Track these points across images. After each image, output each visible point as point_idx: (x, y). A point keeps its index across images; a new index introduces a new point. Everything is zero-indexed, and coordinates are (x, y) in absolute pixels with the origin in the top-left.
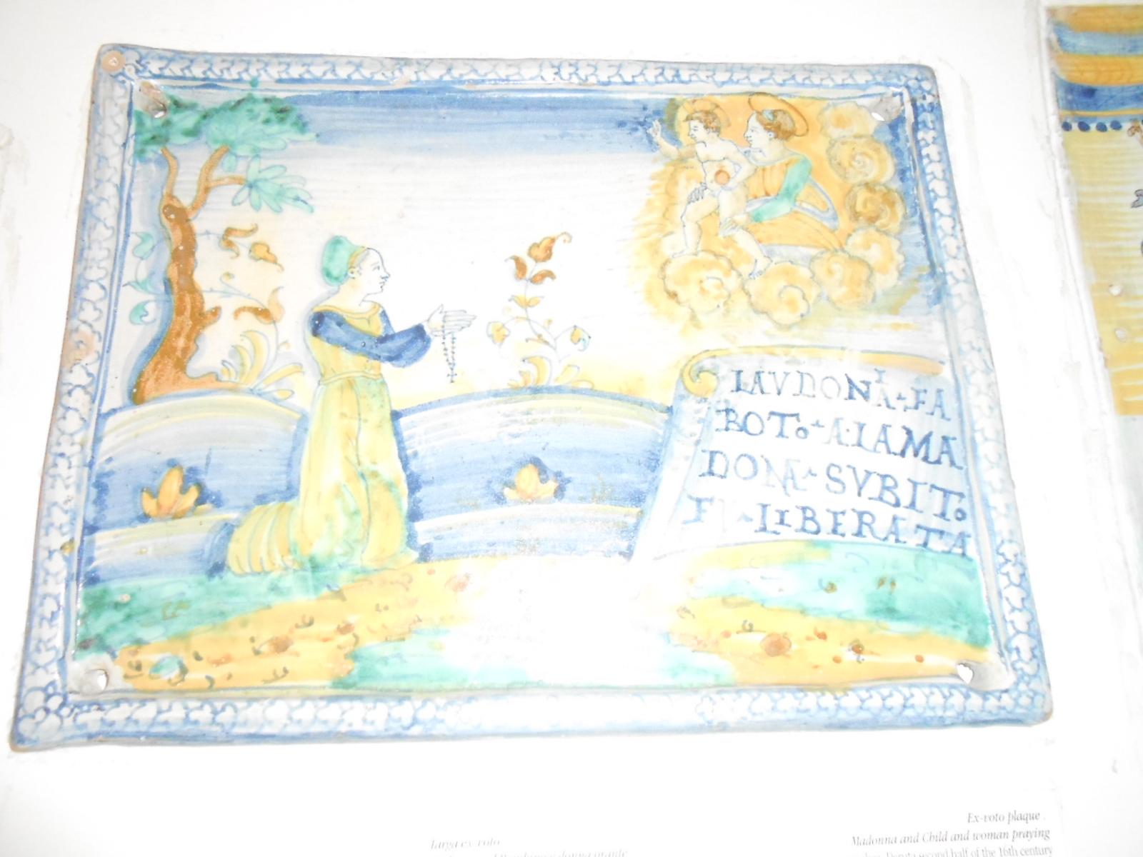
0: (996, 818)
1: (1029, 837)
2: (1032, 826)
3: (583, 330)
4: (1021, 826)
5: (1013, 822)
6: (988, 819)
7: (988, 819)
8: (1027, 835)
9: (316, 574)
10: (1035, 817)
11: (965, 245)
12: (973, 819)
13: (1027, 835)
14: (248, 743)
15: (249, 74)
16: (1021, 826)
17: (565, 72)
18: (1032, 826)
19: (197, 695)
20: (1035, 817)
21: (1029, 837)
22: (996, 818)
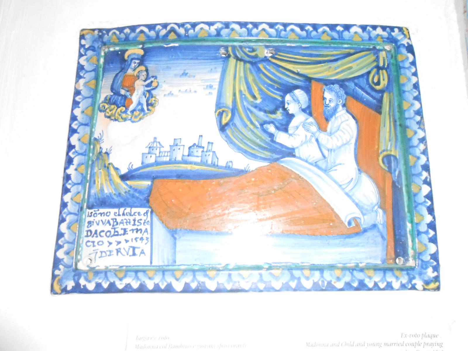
0: (416, 336)
1: (437, 343)
2: (434, 340)
3: (110, 266)
4: (428, 340)
5: (424, 338)
6: (411, 336)
7: (411, 336)
8: (432, 345)
9: (107, 204)
10: (435, 336)
11: (258, 268)
12: (404, 336)
13: (432, 345)
14: (332, 63)
15: (316, 132)
16: (428, 340)
17: (422, 147)
18: (434, 340)
19: (345, 41)
20: (435, 336)
21: (437, 343)
22: (416, 336)
